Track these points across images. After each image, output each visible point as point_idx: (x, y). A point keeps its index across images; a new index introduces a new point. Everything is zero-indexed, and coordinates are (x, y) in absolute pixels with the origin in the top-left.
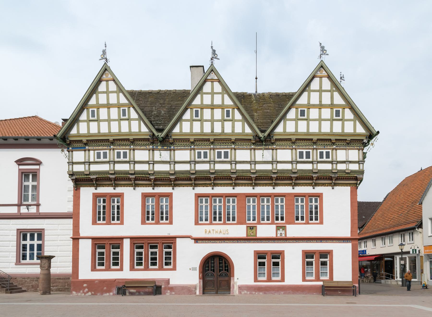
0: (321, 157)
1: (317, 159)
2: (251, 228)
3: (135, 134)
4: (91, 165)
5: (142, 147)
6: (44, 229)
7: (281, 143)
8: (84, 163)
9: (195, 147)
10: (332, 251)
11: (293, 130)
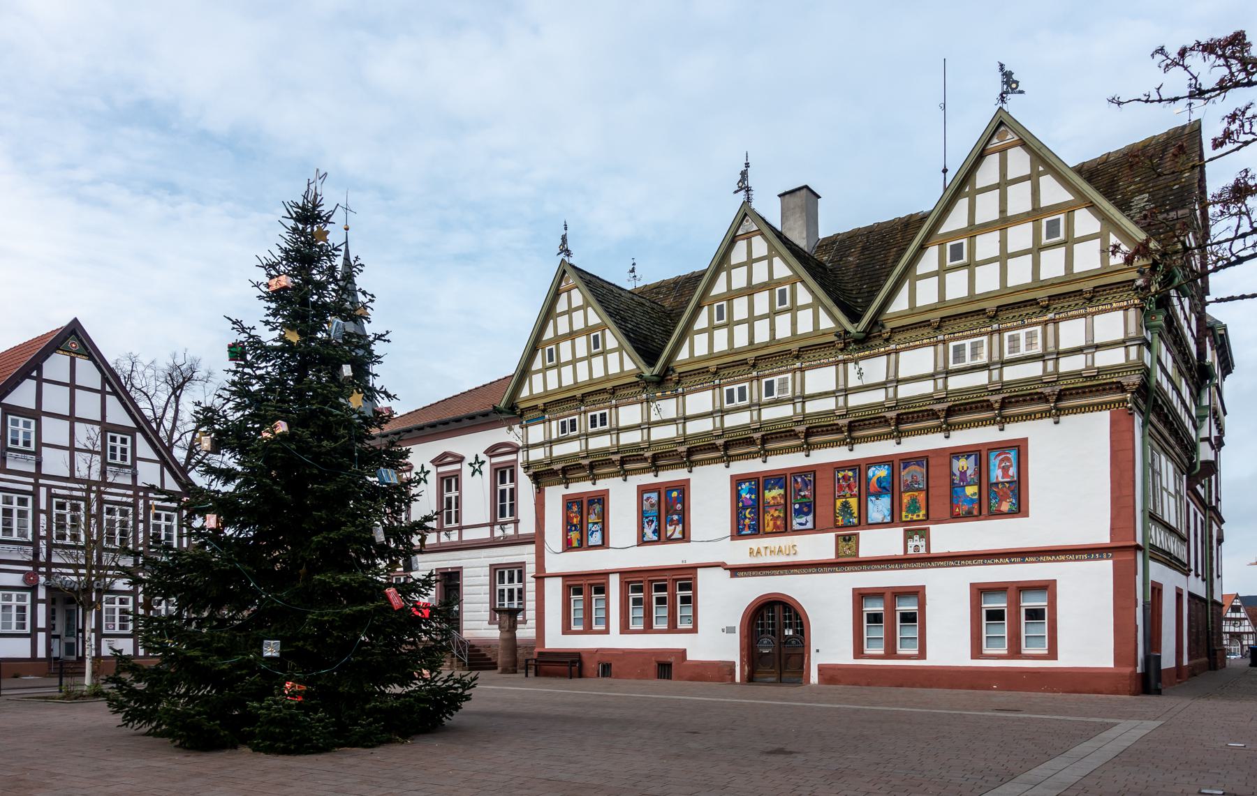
3: (617, 377)
4: (850, 397)
7: (907, 335)
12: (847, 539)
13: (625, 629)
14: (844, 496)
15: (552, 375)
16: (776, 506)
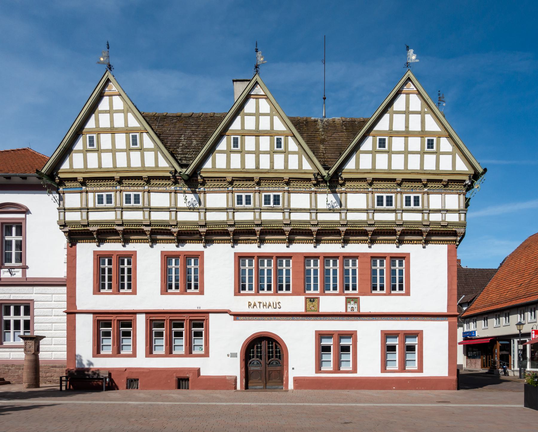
0: (408, 203)
1: (402, 206)
2: (312, 300)
5: (160, 189)
6: (32, 300)
8: (80, 209)
9: (234, 189)
10: (422, 331)
11: (385, 167)
13: (150, 352)
15: (92, 158)
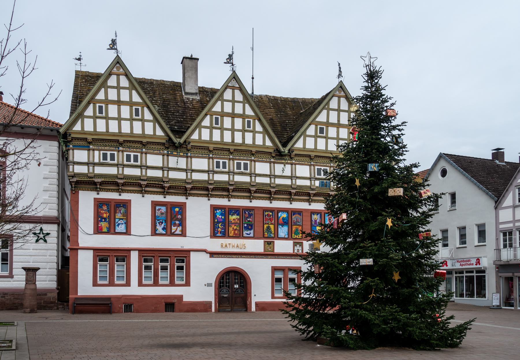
5: (155, 152)
12: (269, 243)
13: (140, 284)
14: (268, 224)
16: (235, 224)
